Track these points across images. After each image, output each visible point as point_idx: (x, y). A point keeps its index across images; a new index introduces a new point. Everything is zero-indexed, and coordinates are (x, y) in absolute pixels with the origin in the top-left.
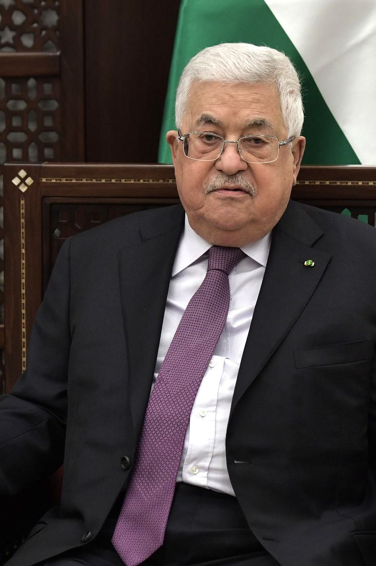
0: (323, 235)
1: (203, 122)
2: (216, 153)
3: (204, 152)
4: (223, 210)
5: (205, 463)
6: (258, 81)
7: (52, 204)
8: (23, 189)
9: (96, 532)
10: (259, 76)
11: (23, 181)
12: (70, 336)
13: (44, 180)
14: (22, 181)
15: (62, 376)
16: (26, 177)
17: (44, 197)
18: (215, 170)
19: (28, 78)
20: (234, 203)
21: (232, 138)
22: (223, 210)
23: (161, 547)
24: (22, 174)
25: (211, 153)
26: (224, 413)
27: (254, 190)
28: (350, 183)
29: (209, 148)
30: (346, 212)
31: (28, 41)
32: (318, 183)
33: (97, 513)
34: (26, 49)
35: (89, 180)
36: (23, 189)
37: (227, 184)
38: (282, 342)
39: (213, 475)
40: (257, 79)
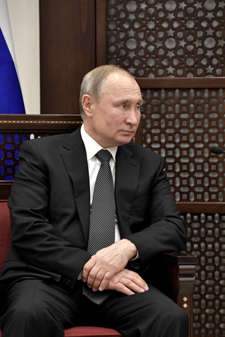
35: (105, 168)
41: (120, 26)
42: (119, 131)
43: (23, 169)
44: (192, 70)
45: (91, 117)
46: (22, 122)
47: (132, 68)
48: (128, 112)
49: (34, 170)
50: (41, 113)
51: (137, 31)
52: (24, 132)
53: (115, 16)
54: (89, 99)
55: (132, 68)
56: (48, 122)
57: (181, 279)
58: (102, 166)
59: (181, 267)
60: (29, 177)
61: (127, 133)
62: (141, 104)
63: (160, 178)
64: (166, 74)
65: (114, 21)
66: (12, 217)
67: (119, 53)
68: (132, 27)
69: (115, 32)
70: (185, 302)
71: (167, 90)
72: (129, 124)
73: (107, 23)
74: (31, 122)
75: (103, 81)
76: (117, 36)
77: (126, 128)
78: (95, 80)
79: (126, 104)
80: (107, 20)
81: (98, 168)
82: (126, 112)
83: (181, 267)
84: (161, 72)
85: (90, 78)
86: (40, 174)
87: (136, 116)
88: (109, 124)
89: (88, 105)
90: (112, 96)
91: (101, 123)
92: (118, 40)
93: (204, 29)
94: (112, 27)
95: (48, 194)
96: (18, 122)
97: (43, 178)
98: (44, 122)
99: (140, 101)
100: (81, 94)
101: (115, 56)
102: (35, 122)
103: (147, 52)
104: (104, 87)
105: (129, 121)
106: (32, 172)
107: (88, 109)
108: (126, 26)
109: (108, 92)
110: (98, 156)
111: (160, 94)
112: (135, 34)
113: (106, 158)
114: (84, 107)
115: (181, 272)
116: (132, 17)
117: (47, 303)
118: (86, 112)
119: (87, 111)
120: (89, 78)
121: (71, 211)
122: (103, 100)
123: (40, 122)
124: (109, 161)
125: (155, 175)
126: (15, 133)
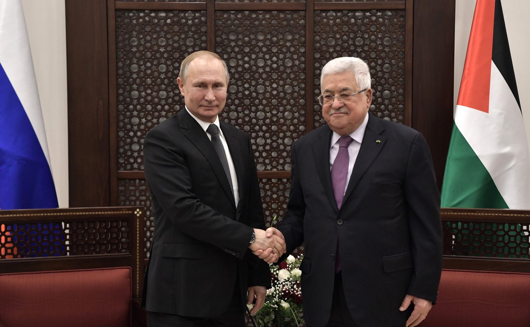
0: (384, 130)
1: (325, 92)
2: (331, 102)
3: (327, 101)
4: (336, 121)
6: (344, 71)
8: (138, 215)
10: (344, 69)
18: (332, 109)
20: (339, 118)
21: (336, 95)
22: (336, 121)
25: (329, 102)
27: (348, 112)
28: (508, 215)
29: (329, 100)
36: (138, 215)
37: (336, 112)
40: (343, 70)
41: (128, 160)
47: (135, 111)
50: (70, 206)
51: (139, 112)
52: (57, 221)
53: (123, 153)
55: (135, 111)
56: (75, 214)
67: (126, 127)
68: (135, 161)
69: (123, 139)
74: (62, 214)
92: (124, 40)
96: (52, 214)
98: (71, 213)
101: (123, 155)
102: (65, 214)
108: (132, 161)
112: (138, 166)
116: (135, 128)
123: (68, 214)
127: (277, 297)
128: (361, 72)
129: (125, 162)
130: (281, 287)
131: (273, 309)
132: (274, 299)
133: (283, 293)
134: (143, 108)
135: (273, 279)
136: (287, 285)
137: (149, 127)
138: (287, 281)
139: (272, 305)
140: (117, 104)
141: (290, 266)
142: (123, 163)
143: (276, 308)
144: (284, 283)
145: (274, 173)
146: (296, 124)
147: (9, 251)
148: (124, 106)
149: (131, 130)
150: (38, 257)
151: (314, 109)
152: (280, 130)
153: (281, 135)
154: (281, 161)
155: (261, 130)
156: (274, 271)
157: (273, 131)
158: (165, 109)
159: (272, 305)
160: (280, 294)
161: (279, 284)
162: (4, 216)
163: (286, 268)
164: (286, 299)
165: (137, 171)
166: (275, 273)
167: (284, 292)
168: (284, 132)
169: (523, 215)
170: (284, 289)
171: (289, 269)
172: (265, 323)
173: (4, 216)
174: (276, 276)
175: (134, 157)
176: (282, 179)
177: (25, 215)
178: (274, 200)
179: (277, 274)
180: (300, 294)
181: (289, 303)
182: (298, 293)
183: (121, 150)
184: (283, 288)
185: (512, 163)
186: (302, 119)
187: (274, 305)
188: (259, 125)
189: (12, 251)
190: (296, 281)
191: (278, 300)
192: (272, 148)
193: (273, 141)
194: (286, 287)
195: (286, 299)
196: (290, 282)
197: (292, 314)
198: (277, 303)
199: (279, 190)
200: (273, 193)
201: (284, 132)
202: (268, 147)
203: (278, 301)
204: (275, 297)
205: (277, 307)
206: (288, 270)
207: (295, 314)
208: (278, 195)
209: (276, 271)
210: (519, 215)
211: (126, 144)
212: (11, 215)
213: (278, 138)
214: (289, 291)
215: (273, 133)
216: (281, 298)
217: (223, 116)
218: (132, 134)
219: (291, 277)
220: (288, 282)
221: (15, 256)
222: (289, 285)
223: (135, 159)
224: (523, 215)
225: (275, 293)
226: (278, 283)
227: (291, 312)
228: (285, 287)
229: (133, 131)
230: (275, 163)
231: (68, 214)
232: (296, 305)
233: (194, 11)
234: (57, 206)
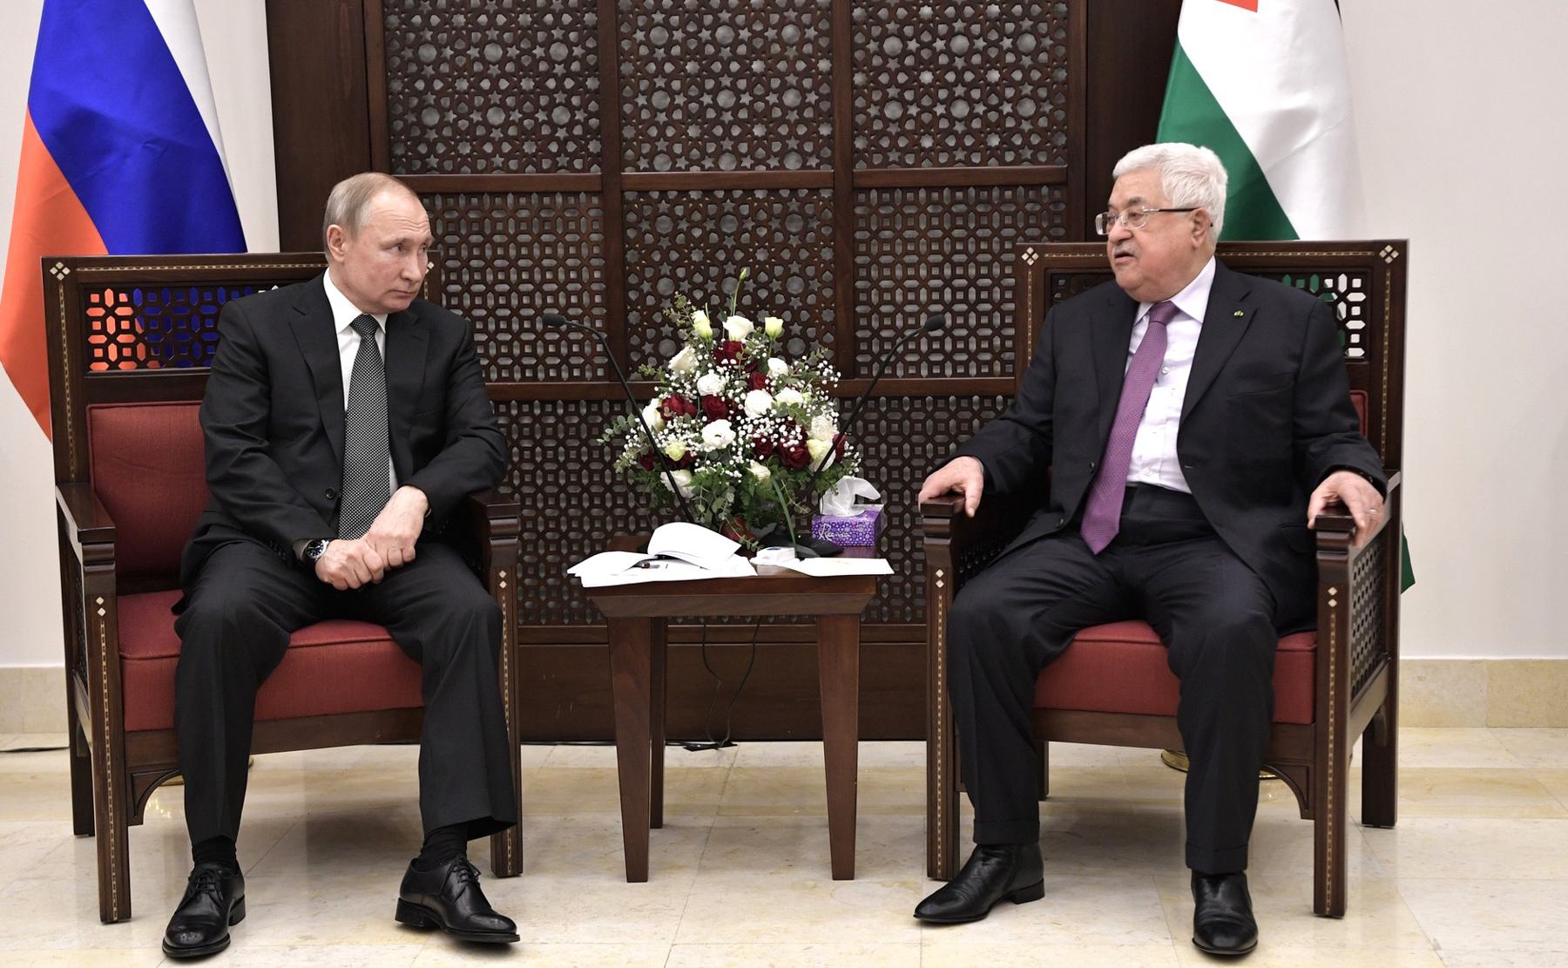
5: (1157, 467)
7: (1052, 275)
8: (1030, 262)
9: (1069, 519)
11: (1030, 256)
12: (1055, 376)
13: (1047, 255)
14: (1029, 257)
15: (1048, 407)
16: (57, 274)
17: (1046, 269)
19: (1042, 185)
23: (1117, 536)
24: (1030, 250)
26: (1173, 429)
30: (1287, 279)
31: (1042, 158)
32: (1264, 254)
33: (1071, 506)
34: (1041, 163)
35: (366, 346)
36: (1030, 262)
38: (1217, 376)
39: (1164, 477)
42: (390, 291)
43: (222, 353)
44: (534, 160)
45: (343, 263)
46: (229, 267)
48: (407, 258)
49: (240, 357)
54: (339, 233)
57: (493, 542)
58: (363, 342)
59: (493, 522)
60: (234, 369)
61: (404, 294)
62: (430, 243)
63: (462, 359)
64: (490, 168)
65: (399, 78)
66: (205, 435)
69: (401, 97)
70: (502, 580)
71: (493, 194)
72: (407, 279)
73: (387, 81)
75: (366, 205)
76: (405, 103)
77: (403, 286)
78: (351, 201)
79: (402, 246)
80: (387, 76)
81: (356, 346)
82: (402, 259)
83: (493, 522)
84: (481, 164)
85: (343, 196)
86: (251, 363)
87: (419, 265)
88: (372, 279)
89: (338, 242)
90: (378, 232)
91: (359, 275)
93: (569, 74)
94: (397, 86)
95: (267, 396)
96: (222, 267)
97: (258, 370)
99: (427, 239)
100: (325, 224)
102: (252, 267)
103: (456, 130)
104: (366, 215)
105: (406, 274)
106: (237, 360)
107: (337, 249)
109: (374, 224)
110: (354, 325)
111: (481, 200)
113: (368, 330)
114: (330, 245)
115: (493, 531)
116: (430, 70)
117: (257, 591)
118: (334, 254)
119: (334, 253)
120: (341, 193)
121: (312, 422)
122: (364, 238)
123: (260, 266)
124: (374, 335)
125: (454, 355)
126: (219, 286)
127: (740, 453)
128: (1178, 170)
129: (407, 152)
130: (750, 430)
131: (733, 481)
132: (734, 457)
133: (753, 445)
134: (445, 22)
135: (732, 412)
136: (765, 425)
137: (461, 68)
138: (764, 417)
139: (727, 472)
140: (383, 12)
141: (773, 383)
142: (403, 156)
143: (737, 478)
144: (756, 422)
145: (760, 175)
146: (810, 56)
147: (127, 352)
148: (400, 18)
149: (418, 76)
150: (194, 366)
151: (852, 17)
152: (771, 71)
153: (775, 83)
154: (776, 147)
155: (726, 70)
156: (735, 395)
157: (754, 74)
158: (496, 23)
159: (727, 472)
160: (748, 446)
161: (746, 423)
162: (110, 269)
163: (764, 386)
164: (761, 457)
165: (437, 174)
166: (737, 400)
167: (755, 440)
168: (781, 75)
169: (1325, 254)
170: (756, 436)
171: (772, 389)
172: (714, 514)
173: (110, 269)
174: (740, 407)
175: (427, 142)
176: (778, 190)
177: (158, 268)
178: (762, 240)
179: (743, 402)
180: (793, 446)
181: (769, 467)
182: (790, 443)
183: (399, 125)
184: (753, 432)
185: (1312, 132)
186: (823, 42)
187: (732, 471)
188: (721, 60)
189: (134, 351)
190: (786, 418)
191: (744, 459)
192: (753, 114)
193: (756, 99)
194: (761, 429)
195: (761, 457)
196: (770, 419)
197: (776, 494)
198: (739, 467)
199: (771, 216)
200: (759, 224)
201: (781, 75)
202: (743, 114)
203: (742, 462)
204: (735, 453)
205: (740, 475)
206: (770, 392)
207: (783, 492)
208: (769, 228)
209: (741, 393)
210: (1316, 254)
211: (407, 110)
212: (126, 269)
213: (769, 90)
214: (768, 439)
215: (754, 78)
216: (750, 454)
217: (635, 39)
218: (420, 85)
219: (774, 407)
220: (767, 419)
221: (141, 364)
222: (768, 426)
223: (431, 146)
224: (1325, 254)
225: (734, 444)
226: (742, 422)
227: (774, 488)
228: (758, 431)
229: (424, 78)
230: (761, 152)
231: (260, 266)
232: (784, 471)
233: (1004, 187)
234: (242, 246)
